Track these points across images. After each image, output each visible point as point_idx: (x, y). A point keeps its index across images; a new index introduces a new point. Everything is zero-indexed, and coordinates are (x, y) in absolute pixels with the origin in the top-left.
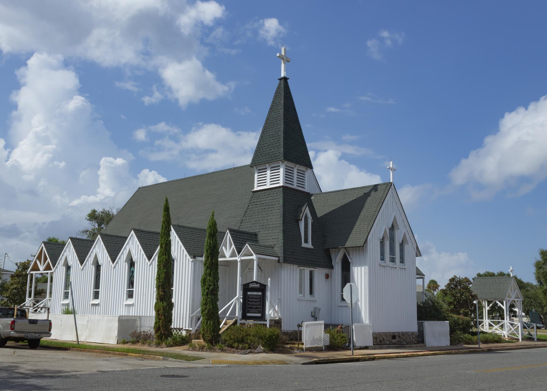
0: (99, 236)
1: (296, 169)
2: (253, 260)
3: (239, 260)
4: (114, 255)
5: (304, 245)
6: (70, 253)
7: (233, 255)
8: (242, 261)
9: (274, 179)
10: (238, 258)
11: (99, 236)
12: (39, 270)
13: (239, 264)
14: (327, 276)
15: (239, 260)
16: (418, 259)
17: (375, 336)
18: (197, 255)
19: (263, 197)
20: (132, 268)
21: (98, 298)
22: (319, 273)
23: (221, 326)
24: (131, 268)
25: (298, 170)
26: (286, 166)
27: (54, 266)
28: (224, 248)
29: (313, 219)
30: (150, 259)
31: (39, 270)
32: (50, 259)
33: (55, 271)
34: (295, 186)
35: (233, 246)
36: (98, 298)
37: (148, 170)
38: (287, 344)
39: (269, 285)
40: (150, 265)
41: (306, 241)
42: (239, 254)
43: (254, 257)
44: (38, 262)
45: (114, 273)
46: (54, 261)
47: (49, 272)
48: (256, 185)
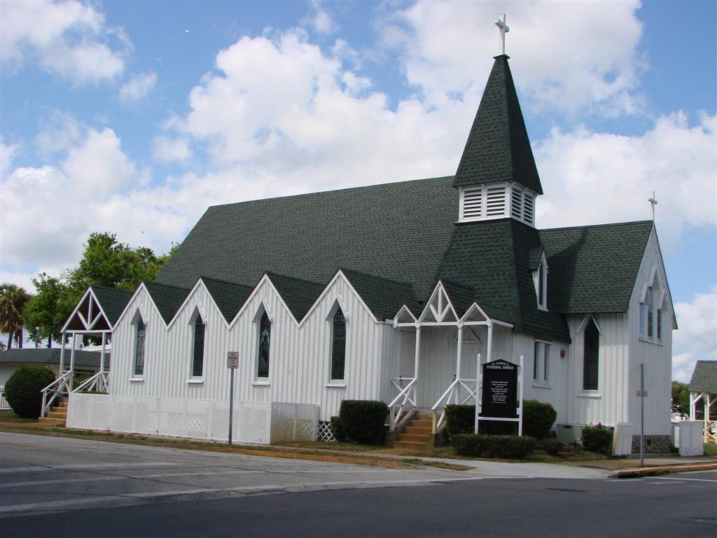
0: (142, 284)
1: (524, 193)
2: (486, 327)
3: (460, 326)
4: (168, 313)
5: (540, 307)
6: (143, 302)
7: (449, 317)
8: (422, 327)
9: (495, 207)
10: (459, 323)
11: (142, 284)
12: (84, 329)
13: (460, 332)
14: (563, 354)
15: (460, 326)
16: (674, 331)
17: (230, 356)
18: (386, 316)
19: (476, 233)
20: (265, 332)
21: (201, 375)
22: (555, 349)
23: (62, 332)
24: (261, 332)
25: (526, 195)
26: (514, 189)
27: (113, 325)
28: (432, 307)
29: (549, 269)
30: (301, 319)
31: (84, 329)
32: (104, 310)
33: (114, 331)
34: (522, 220)
35: (450, 305)
36: (201, 375)
37: (508, 60)
38: (5, 313)
39: (521, 364)
40: (300, 328)
41: (541, 303)
42: (460, 317)
43: (489, 322)
44: (80, 315)
45: (231, 337)
46: (115, 316)
47: (104, 331)
48: (461, 214)
